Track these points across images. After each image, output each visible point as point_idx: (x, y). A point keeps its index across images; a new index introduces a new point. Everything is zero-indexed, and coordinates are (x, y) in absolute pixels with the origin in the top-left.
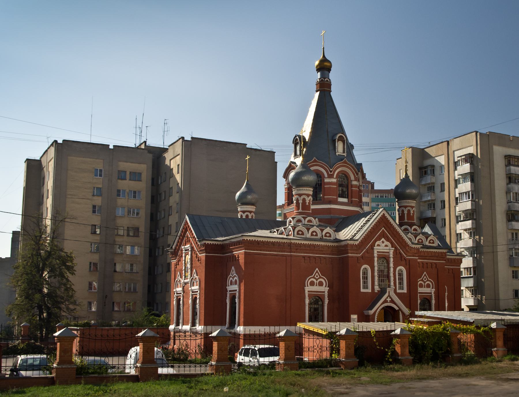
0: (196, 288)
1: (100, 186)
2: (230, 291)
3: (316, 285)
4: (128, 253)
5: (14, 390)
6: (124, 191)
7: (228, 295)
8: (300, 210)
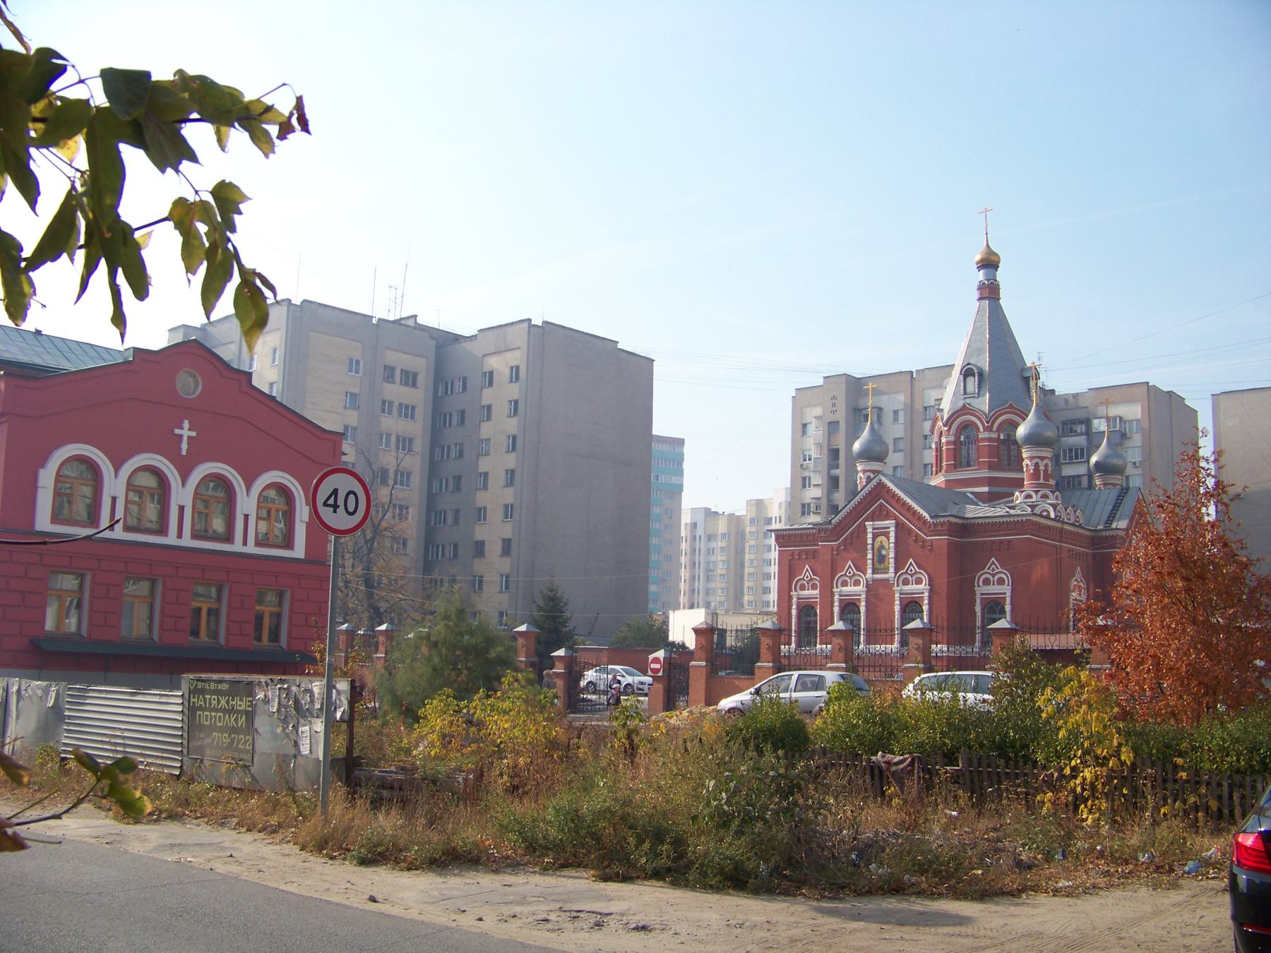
0: (921, 588)
1: (356, 391)
6: (391, 403)
7: (978, 601)
8: (1041, 481)
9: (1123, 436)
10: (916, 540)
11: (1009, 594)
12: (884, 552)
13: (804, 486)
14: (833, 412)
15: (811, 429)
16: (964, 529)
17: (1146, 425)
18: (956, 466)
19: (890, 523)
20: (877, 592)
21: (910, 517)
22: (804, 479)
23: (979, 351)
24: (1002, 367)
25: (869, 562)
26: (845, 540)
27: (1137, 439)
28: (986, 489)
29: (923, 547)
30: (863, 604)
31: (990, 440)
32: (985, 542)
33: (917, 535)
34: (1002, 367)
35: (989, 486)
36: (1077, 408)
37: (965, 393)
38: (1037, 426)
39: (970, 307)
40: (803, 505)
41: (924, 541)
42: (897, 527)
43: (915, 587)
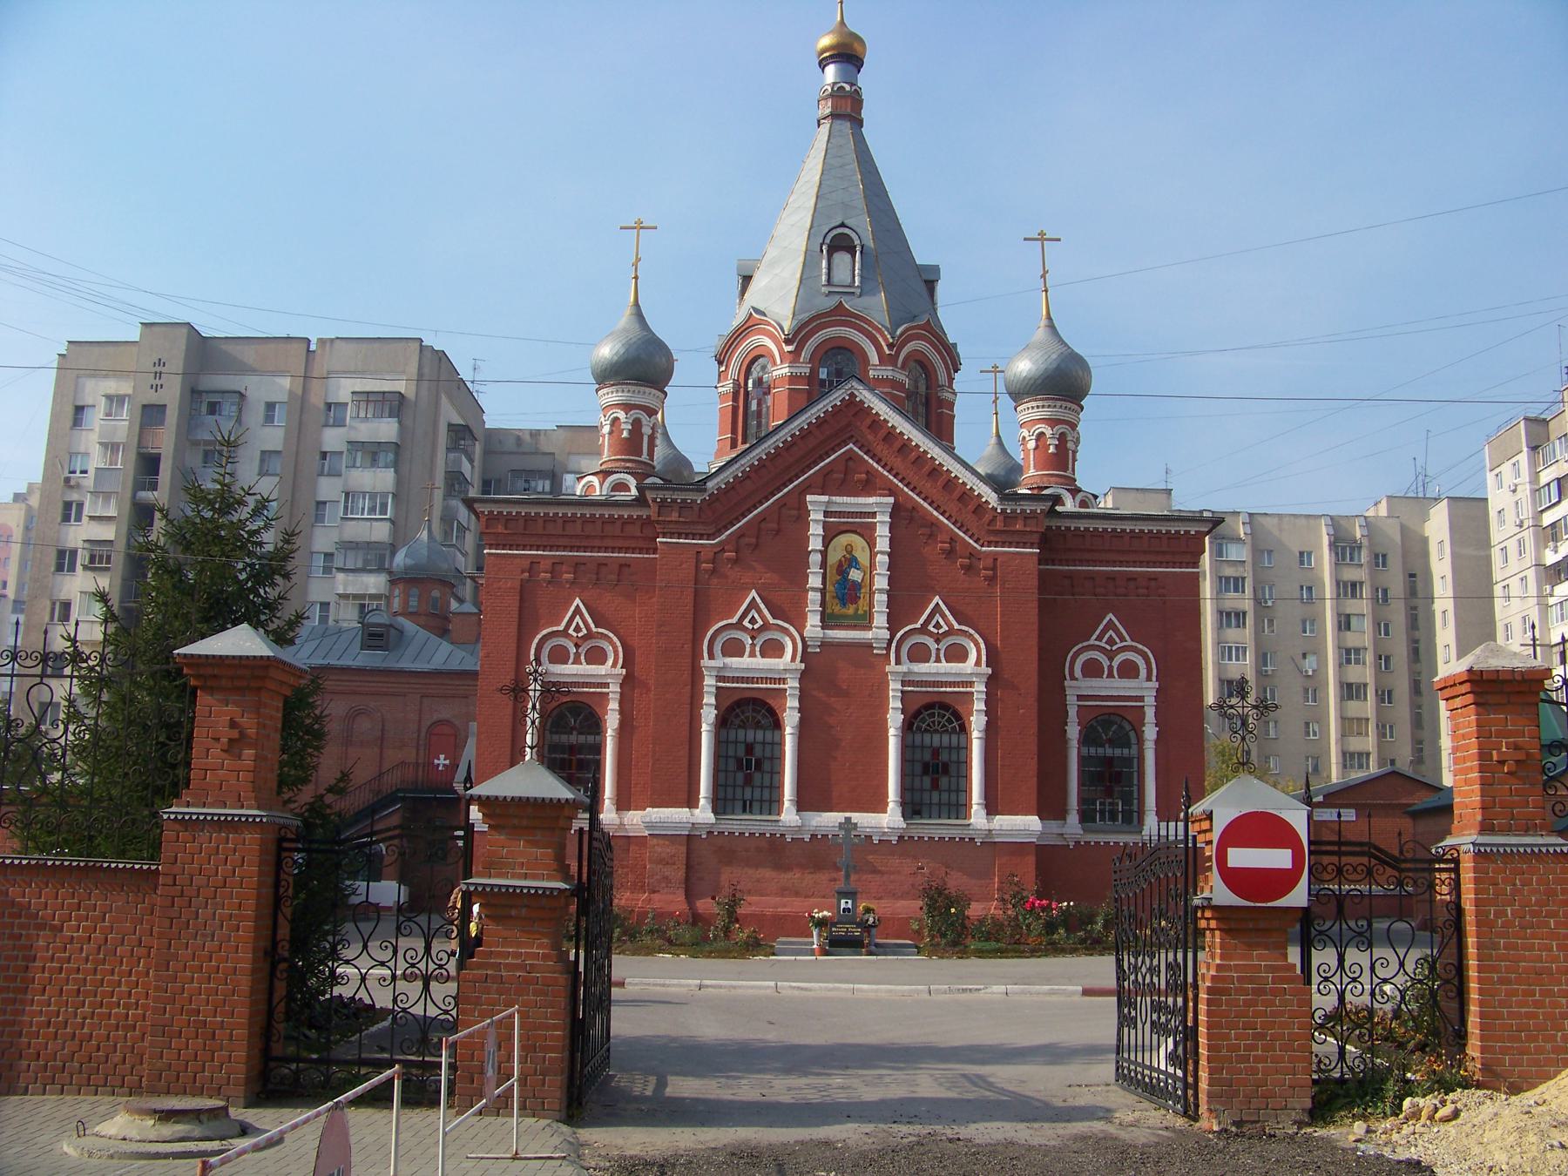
2: (1080, 698)
3: (1110, 675)
10: (950, 554)
11: (1150, 701)
12: (855, 575)
13: (66, 518)
15: (96, 419)
19: (878, 506)
20: (834, 679)
22: (68, 505)
26: (740, 535)
29: (968, 569)
30: (792, 702)
33: (953, 539)
36: (536, 453)
40: (61, 553)
41: (973, 554)
43: (945, 666)
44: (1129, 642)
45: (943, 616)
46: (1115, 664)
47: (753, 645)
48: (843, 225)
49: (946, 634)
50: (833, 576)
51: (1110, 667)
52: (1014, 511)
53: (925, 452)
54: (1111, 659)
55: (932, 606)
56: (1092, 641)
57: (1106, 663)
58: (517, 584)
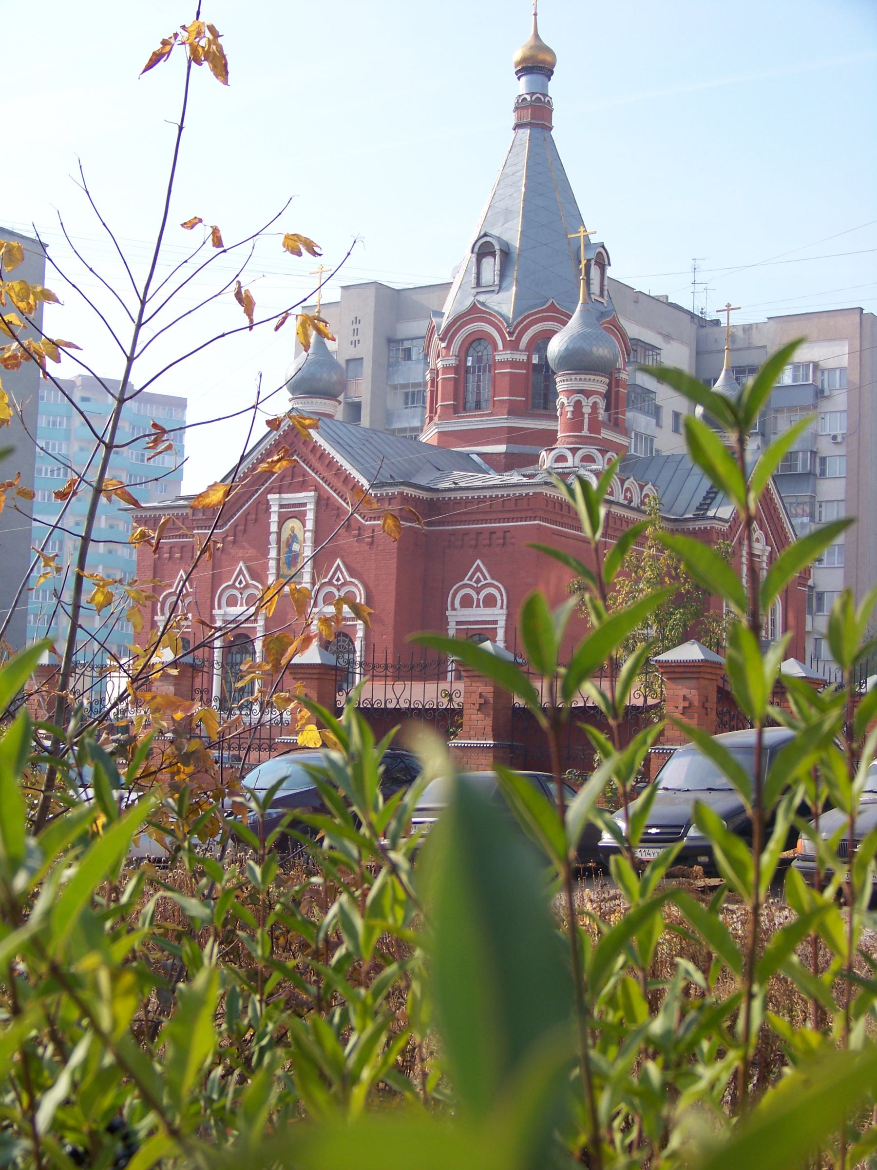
2: (458, 623)
3: (478, 606)
4: (497, 358)
5: (275, 1117)
8: (585, 432)
9: (820, 394)
10: (348, 526)
11: (502, 623)
12: (296, 547)
14: (355, 343)
16: (432, 507)
17: (856, 378)
18: (459, 408)
19: (307, 497)
21: (339, 485)
23: (507, 214)
24: (545, 241)
25: (272, 564)
26: (236, 526)
27: (840, 400)
28: (502, 448)
31: (513, 364)
32: (466, 533)
34: (545, 241)
35: (509, 441)
37: (478, 284)
38: (582, 336)
39: (499, 140)
42: (318, 503)
44: (489, 580)
45: (342, 573)
46: (481, 597)
47: (242, 598)
48: (485, 235)
49: (343, 585)
50: (284, 549)
51: (478, 600)
52: (382, 495)
53: (333, 458)
54: (478, 594)
55: (335, 566)
56: (466, 581)
57: (475, 596)
58: (152, 563)
